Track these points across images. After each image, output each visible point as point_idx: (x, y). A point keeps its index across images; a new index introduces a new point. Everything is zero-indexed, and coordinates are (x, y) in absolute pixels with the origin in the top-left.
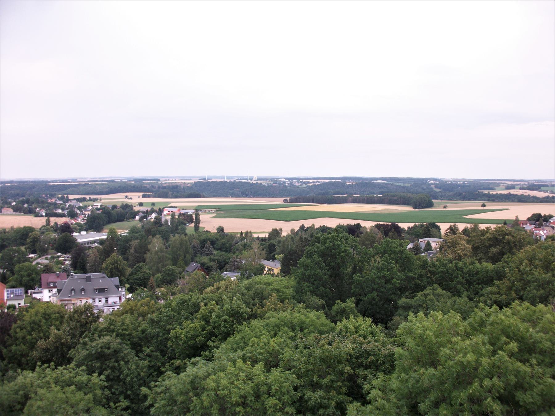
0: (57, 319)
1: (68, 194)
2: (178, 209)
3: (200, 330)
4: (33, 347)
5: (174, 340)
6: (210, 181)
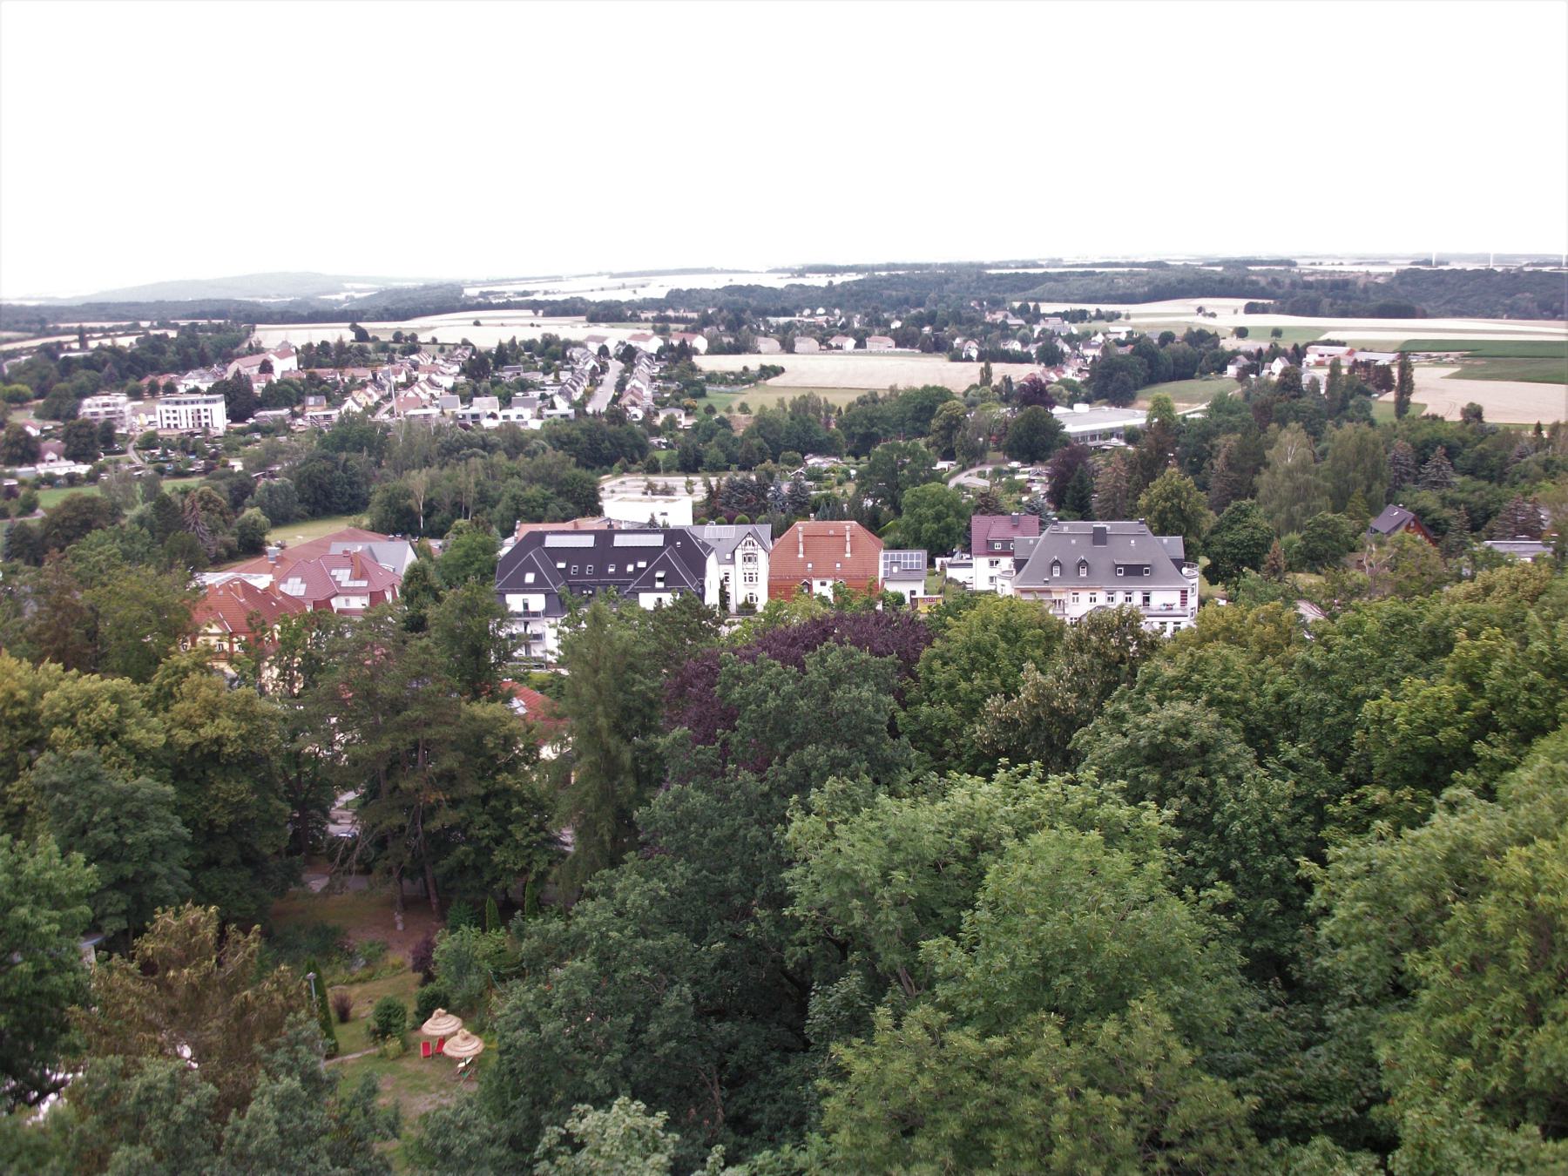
0: (1037, 643)
1: (1037, 300)
2: (1347, 349)
3: (1454, 707)
4: (975, 712)
5: (1372, 729)
6: (1446, 268)
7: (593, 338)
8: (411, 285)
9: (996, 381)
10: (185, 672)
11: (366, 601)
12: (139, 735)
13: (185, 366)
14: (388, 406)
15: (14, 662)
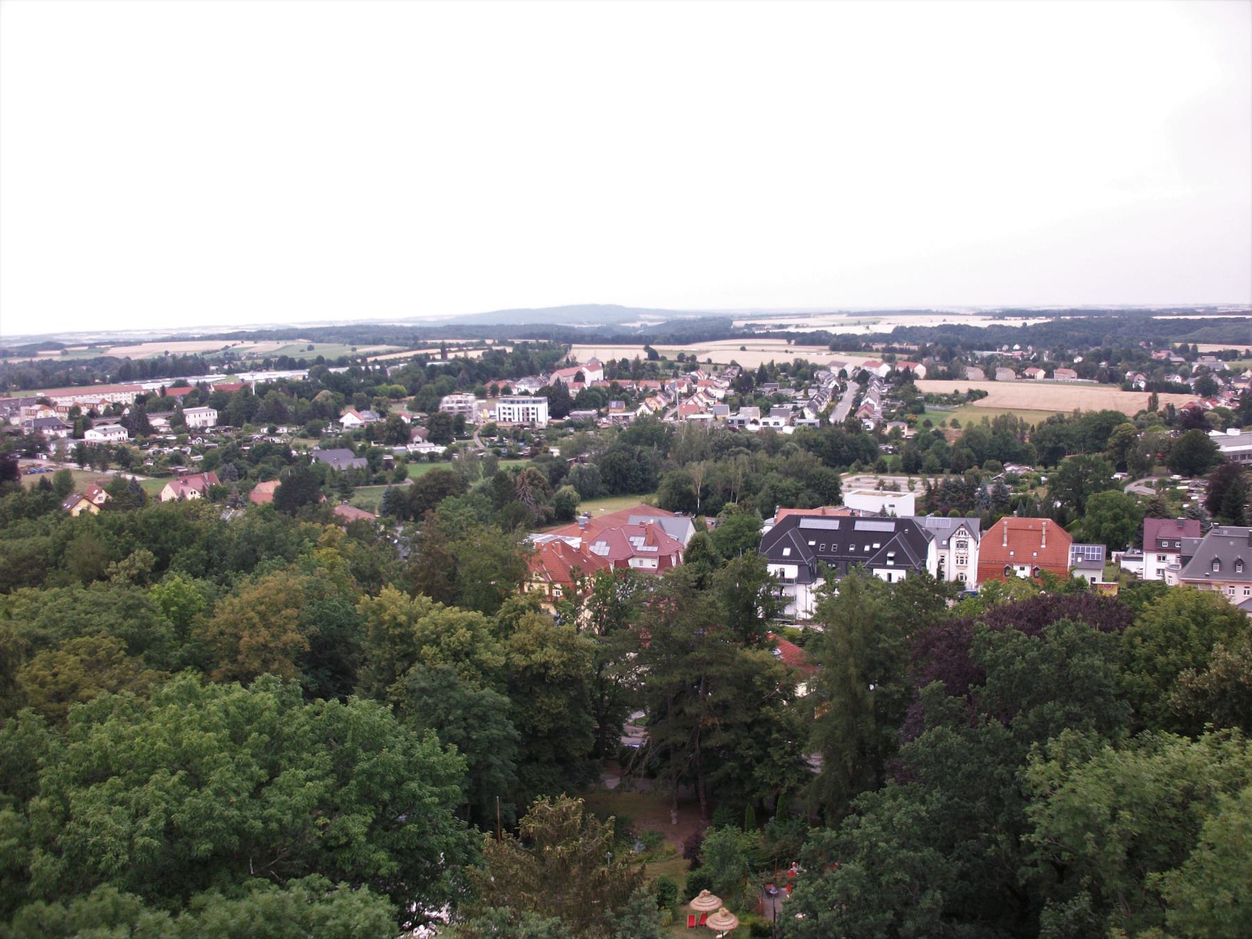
0: (1222, 627)
4: (1169, 681)
7: (834, 364)
8: (692, 317)
9: (1161, 408)
10: (523, 610)
11: (656, 562)
12: (486, 656)
13: (518, 374)
14: (673, 411)
15: (397, 593)
